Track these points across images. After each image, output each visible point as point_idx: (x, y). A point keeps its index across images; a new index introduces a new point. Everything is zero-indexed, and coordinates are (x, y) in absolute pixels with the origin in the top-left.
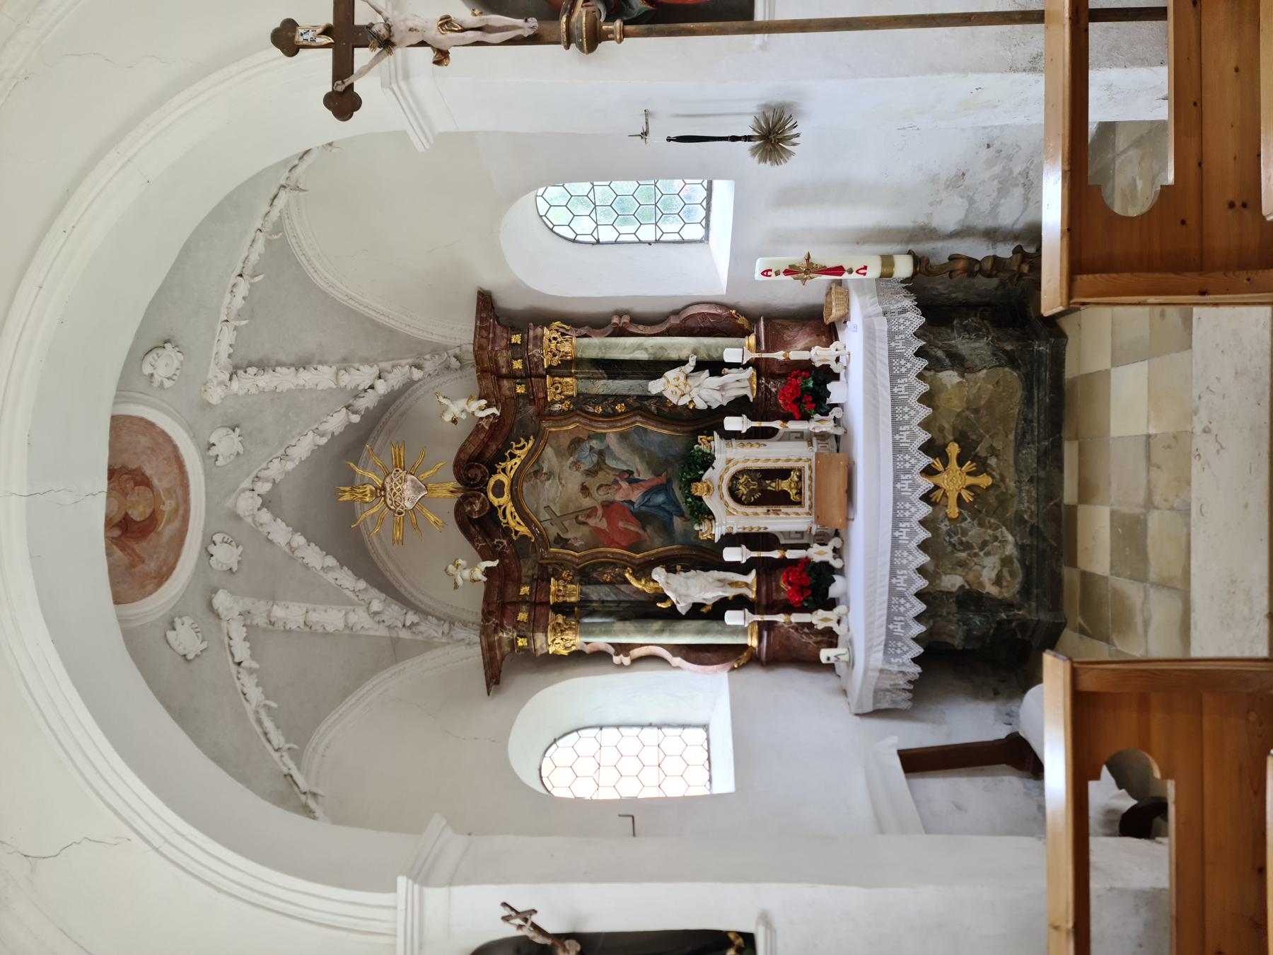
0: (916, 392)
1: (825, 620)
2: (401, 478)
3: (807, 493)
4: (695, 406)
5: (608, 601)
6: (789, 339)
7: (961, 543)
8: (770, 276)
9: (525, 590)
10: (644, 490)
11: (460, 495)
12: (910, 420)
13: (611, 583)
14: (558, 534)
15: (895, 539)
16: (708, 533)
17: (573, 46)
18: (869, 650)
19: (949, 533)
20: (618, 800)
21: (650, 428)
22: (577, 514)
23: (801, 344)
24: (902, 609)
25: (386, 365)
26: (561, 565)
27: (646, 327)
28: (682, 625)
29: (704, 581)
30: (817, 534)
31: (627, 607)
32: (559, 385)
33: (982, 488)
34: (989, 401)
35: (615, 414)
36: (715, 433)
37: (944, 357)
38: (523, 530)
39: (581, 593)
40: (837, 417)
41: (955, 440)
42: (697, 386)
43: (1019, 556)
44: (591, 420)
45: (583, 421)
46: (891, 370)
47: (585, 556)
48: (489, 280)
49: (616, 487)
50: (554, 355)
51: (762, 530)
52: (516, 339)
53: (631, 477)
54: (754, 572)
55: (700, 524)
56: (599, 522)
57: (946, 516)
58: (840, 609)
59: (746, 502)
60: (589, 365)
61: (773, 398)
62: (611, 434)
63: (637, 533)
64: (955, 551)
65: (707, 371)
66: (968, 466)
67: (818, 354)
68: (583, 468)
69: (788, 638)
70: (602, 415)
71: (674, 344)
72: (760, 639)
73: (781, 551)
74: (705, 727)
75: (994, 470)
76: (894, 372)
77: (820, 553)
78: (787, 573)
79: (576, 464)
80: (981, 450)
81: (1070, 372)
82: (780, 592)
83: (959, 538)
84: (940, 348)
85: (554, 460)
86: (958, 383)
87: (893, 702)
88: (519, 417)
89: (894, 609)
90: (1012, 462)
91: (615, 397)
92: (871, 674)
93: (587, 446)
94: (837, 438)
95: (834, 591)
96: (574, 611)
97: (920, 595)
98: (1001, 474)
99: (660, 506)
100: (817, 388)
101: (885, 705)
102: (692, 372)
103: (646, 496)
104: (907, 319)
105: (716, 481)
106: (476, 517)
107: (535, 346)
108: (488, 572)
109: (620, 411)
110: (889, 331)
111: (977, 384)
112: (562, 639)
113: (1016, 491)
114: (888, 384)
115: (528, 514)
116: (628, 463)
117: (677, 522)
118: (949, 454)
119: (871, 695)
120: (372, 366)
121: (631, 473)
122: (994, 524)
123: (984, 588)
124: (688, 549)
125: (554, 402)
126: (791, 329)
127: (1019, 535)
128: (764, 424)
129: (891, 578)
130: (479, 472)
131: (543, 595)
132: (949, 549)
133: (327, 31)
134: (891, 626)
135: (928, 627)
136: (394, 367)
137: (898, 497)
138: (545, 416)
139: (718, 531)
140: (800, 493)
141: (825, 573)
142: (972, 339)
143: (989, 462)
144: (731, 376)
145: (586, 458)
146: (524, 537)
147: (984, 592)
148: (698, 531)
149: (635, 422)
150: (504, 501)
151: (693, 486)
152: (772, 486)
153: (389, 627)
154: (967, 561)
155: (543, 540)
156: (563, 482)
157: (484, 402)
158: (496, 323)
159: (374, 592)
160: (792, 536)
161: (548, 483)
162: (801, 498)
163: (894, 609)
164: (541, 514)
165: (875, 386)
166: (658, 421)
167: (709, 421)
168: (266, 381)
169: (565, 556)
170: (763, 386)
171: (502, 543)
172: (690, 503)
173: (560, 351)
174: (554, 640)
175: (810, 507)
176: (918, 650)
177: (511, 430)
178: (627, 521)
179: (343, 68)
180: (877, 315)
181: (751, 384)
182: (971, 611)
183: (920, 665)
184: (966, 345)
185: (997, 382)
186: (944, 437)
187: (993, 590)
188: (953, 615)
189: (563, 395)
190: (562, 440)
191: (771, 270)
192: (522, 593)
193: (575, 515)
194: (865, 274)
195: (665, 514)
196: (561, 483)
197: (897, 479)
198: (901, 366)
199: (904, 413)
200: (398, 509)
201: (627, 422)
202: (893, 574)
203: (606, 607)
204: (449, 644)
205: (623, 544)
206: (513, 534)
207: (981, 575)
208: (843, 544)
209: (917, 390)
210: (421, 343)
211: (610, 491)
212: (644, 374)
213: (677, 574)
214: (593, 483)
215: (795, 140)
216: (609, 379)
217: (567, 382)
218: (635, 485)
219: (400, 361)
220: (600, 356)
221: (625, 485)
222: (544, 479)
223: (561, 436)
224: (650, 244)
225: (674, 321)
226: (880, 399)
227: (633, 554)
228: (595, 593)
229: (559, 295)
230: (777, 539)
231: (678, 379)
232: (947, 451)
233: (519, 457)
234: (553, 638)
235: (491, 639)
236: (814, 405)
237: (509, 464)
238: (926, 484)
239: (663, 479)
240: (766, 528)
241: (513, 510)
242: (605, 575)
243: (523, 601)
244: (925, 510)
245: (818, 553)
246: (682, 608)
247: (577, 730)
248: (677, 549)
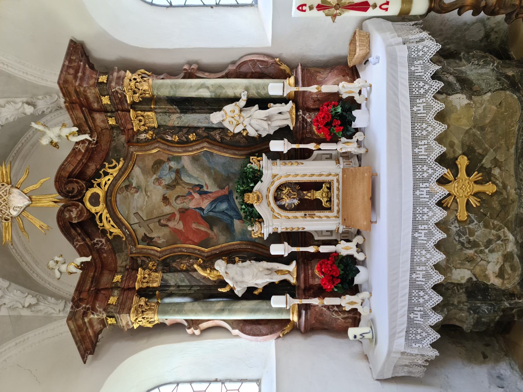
1: (352, 303)
2: (6, 191)
3: (335, 201)
4: (247, 133)
6: (321, 79)
7: (469, 242)
8: (305, 11)
10: (211, 200)
11: (62, 204)
12: (427, 135)
13: (187, 271)
14: (145, 233)
15: (414, 239)
16: (259, 233)
18: (392, 337)
19: (458, 234)
22: (160, 218)
26: (148, 258)
27: (211, 74)
28: (239, 305)
29: (255, 270)
30: (343, 233)
31: (198, 290)
32: (141, 118)
33: (488, 194)
34: (493, 121)
35: (188, 141)
36: (264, 155)
37: (455, 82)
38: (116, 231)
39: (162, 279)
40: (360, 140)
41: (464, 154)
42: (249, 117)
43: (519, 253)
44: (169, 146)
46: (411, 91)
47: (165, 251)
49: (190, 198)
50: (135, 93)
51: (300, 230)
53: (201, 190)
54: (294, 263)
55: (252, 226)
56: (177, 224)
59: (288, 208)
60: (166, 102)
61: (309, 127)
62: (186, 158)
63: (206, 232)
64: (464, 249)
65: (257, 105)
66: (476, 176)
67: (345, 86)
68: (164, 183)
69: (321, 315)
70: (178, 143)
72: (300, 316)
73: (316, 247)
74: (258, 381)
75: (497, 179)
76: (414, 93)
77: (347, 248)
78: (321, 265)
79: (158, 180)
80: (486, 162)
82: (315, 279)
83: (467, 237)
84: (451, 74)
85: (142, 177)
86: (466, 105)
87: (410, 372)
88: (114, 144)
89: (415, 300)
90: (513, 172)
91: (188, 129)
92: (393, 355)
93: (166, 166)
94: (359, 157)
95: (358, 280)
96: (155, 295)
97: (436, 288)
98: (503, 183)
99: (223, 211)
100: (344, 114)
102: (244, 107)
103: (213, 204)
105: (264, 193)
106: (76, 222)
107: (117, 84)
109: (192, 139)
110: (409, 57)
111: (482, 105)
112: (143, 318)
115: (120, 219)
116: (199, 179)
118: (459, 166)
121: (201, 186)
122: (497, 225)
124: (245, 244)
126: (322, 73)
127: (519, 235)
129: (411, 274)
131: (131, 282)
132: (459, 247)
134: (412, 316)
135: (444, 315)
137: (417, 203)
138: (133, 143)
139: (266, 231)
140: (330, 201)
142: (480, 65)
143: (492, 172)
145: (167, 175)
146: (117, 237)
147: (489, 284)
148: (251, 231)
149: (203, 148)
150: (100, 209)
151: (246, 195)
152: (309, 195)
154: (475, 257)
155: (132, 238)
156: (149, 194)
158: (87, 66)
160: (324, 234)
161: (136, 195)
162: (330, 205)
163: (415, 300)
164: (131, 219)
165: (397, 105)
166: (221, 146)
169: (149, 251)
170: (300, 117)
171: (101, 241)
172: (244, 209)
173: (139, 89)
174: (137, 319)
175: (338, 212)
176: (435, 336)
178: (199, 223)
180: (398, 44)
181: (291, 115)
182: (479, 301)
184: (474, 71)
185: (500, 104)
186: (454, 152)
187: (496, 282)
188: (463, 303)
189: (147, 126)
190: (147, 162)
191: (305, 5)
192: (115, 281)
193: (157, 220)
194: (386, 9)
195: (228, 218)
196: (147, 195)
199: (422, 129)
200: (4, 216)
201: (197, 147)
202: (413, 271)
203: (180, 290)
205: (196, 241)
206: (108, 235)
208: (364, 241)
209: (434, 109)
210: (36, 87)
211: (185, 201)
212: (208, 109)
213: (236, 265)
214: (172, 194)
216: (181, 113)
217: (148, 116)
218: (204, 196)
219: (14, 99)
221: (196, 196)
222: (133, 192)
223: (146, 159)
224: (212, 7)
225: (232, 68)
226: (402, 118)
227: (203, 249)
228: (173, 279)
229: (141, 47)
230: (313, 236)
231: (234, 111)
232: (457, 163)
233: (111, 174)
234: (135, 318)
236: (342, 128)
237: (104, 180)
239: (225, 192)
240: (304, 229)
241: (108, 215)
242: (182, 265)
246: (239, 291)
248: (236, 244)
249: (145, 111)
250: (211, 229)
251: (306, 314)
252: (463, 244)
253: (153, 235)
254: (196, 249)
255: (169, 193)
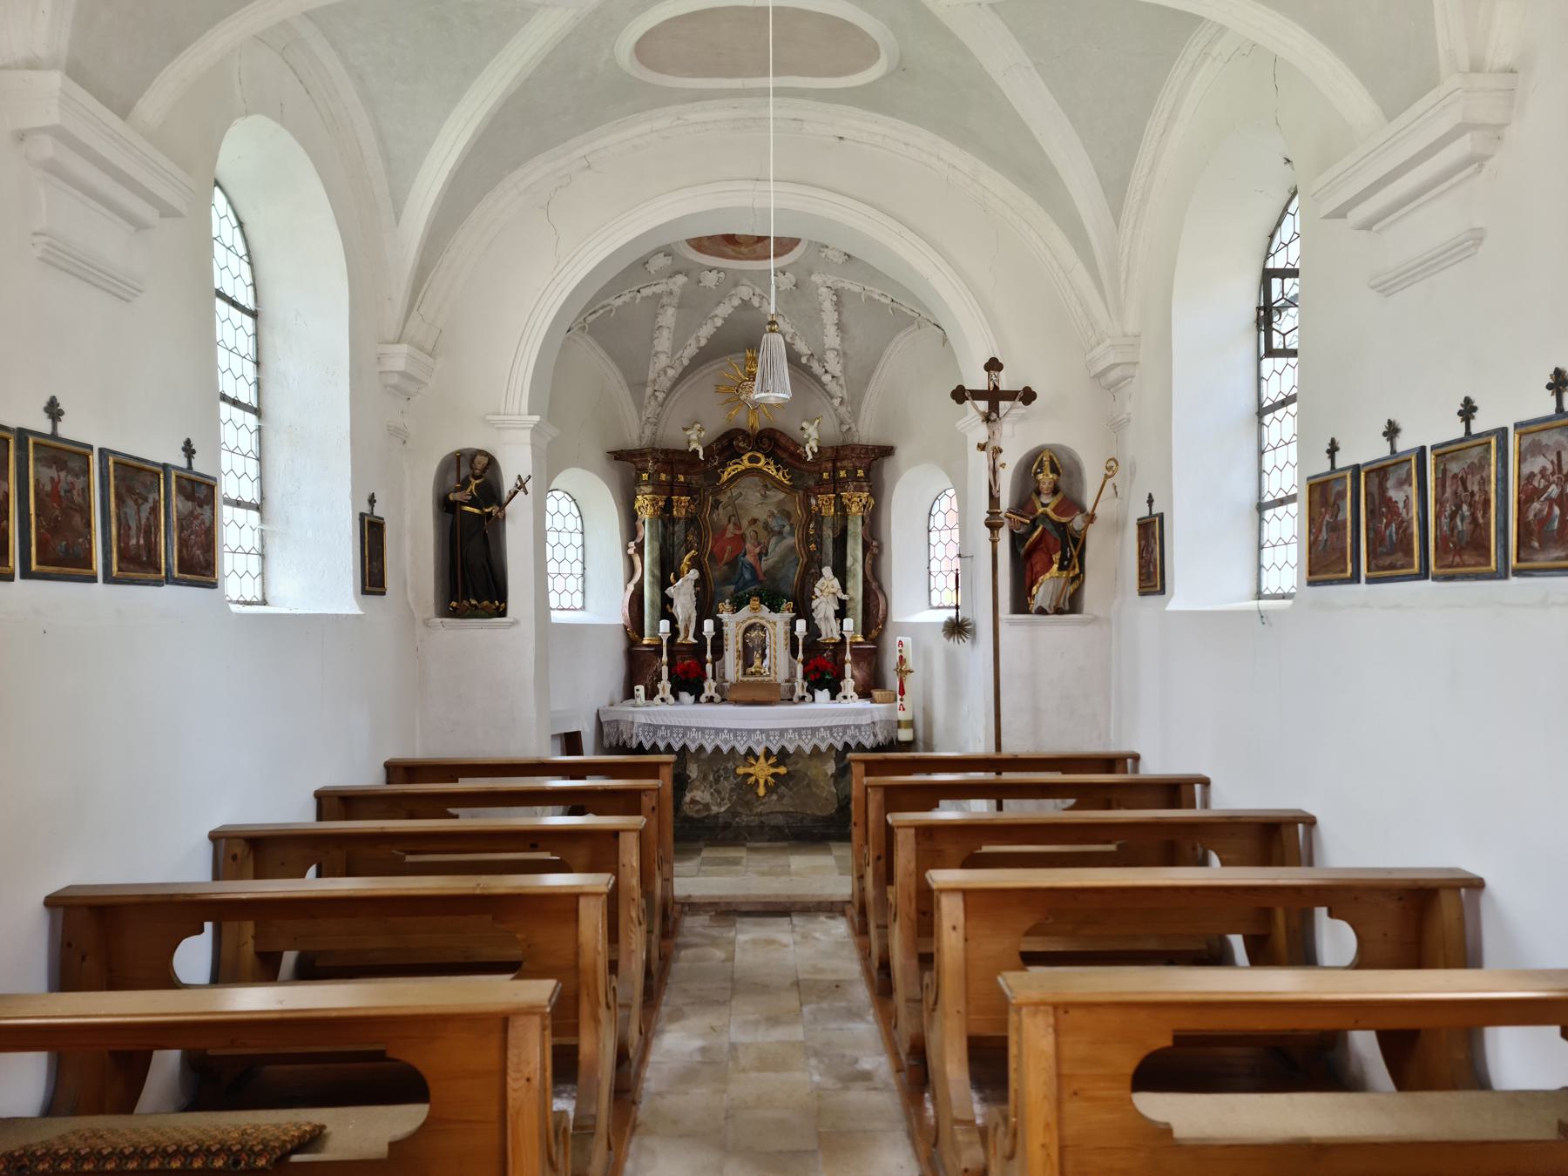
0: (821, 743)
1: (663, 689)
3: (752, 679)
5: (673, 538)
7: (719, 777)
9: (681, 478)
11: (750, 432)
13: (686, 540)
17: (988, 515)
19: (726, 768)
20: (1298, 444)
21: (799, 569)
23: (856, 673)
24: (675, 735)
25: (842, 381)
26: (699, 504)
28: (657, 590)
38: (725, 477)
39: (679, 519)
41: (788, 772)
45: (803, 520)
46: (836, 727)
48: (902, 454)
50: (849, 500)
51: (725, 647)
52: (860, 473)
54: (696, 641)
55: (730, 604)
56: (731, 531)
57: (738, 767)
58: (672, 699)
65: (838, 608)
68: (770, 520)
69: (650, 666)
70: (807, 533)
71: (857, 585)
74: (583, 608)
77: (710, 688)
79: (772, 515)
80: (783, 789)
81: (831, 844)
85: (775, 500)
88: (806, 474)
92: (630, 716)
95: (686, 697)
97: (684, 747)
101: (606, 730)
104: (869, 736)
105: (759, 614)
107: (855, 487)
108: (696, 452)
110: (861, 725)
113: (755, 813)
114: (827, 724)
117: (732, 588)
119: (614, 719)
120: (841, 372)
121: (766, 554)
123: (689, 792)
125: (817, 500)
128: (801, 648)
129: (696, 728)
130: (766, 445)
132: (715, 769)
133: (996, 387)
134: (663, 728)
136: (841, 386)
137: (751, 732)
139: (725, 616)
140: (752, 674)
141: (697, 691)
144: (834, 624)
149: (802, 557)
150: (746, 464)
153: (655, 380)
155: (719, 491)
157: (816, 450)
159: (680, 370)
161: (759, 495)
165: (826, 716)
167: (803, 609)
168: (828, 306)
177: (797, 469)
179: (977, 395)
180: (872, 717)
183: (637, 748)
186: (790, 765)
187: (688, 798)
193: (735, 513)
197: (762, 731)
198: (838, 733)
199: (806, 735)
201: (803, 552)
202: (698, 729)
204: (641, 420)
205: (715, 549)
207: (697, 790)
210: (859, 404)
214: (759, 527)
215: (961, 640)
216: (834, 539)
220: (849, 533)
221: (757, 550)
224: (929, 568)
225: (874, 585)
228: (679, 528)
235: (649, 455)
238: (759, 751)
239: (761, 578)
241: (740, 470)
243: (674, 477)
244: (742, 750)
245: (710, 687)
246: (670, 591)
247: (581, 516)
249: (835, 506)
250: (726, 564)
251: (651, 651)
252: (718, 771)
253: (721, 510)
254: (707, 549)
255: (760, 524)
